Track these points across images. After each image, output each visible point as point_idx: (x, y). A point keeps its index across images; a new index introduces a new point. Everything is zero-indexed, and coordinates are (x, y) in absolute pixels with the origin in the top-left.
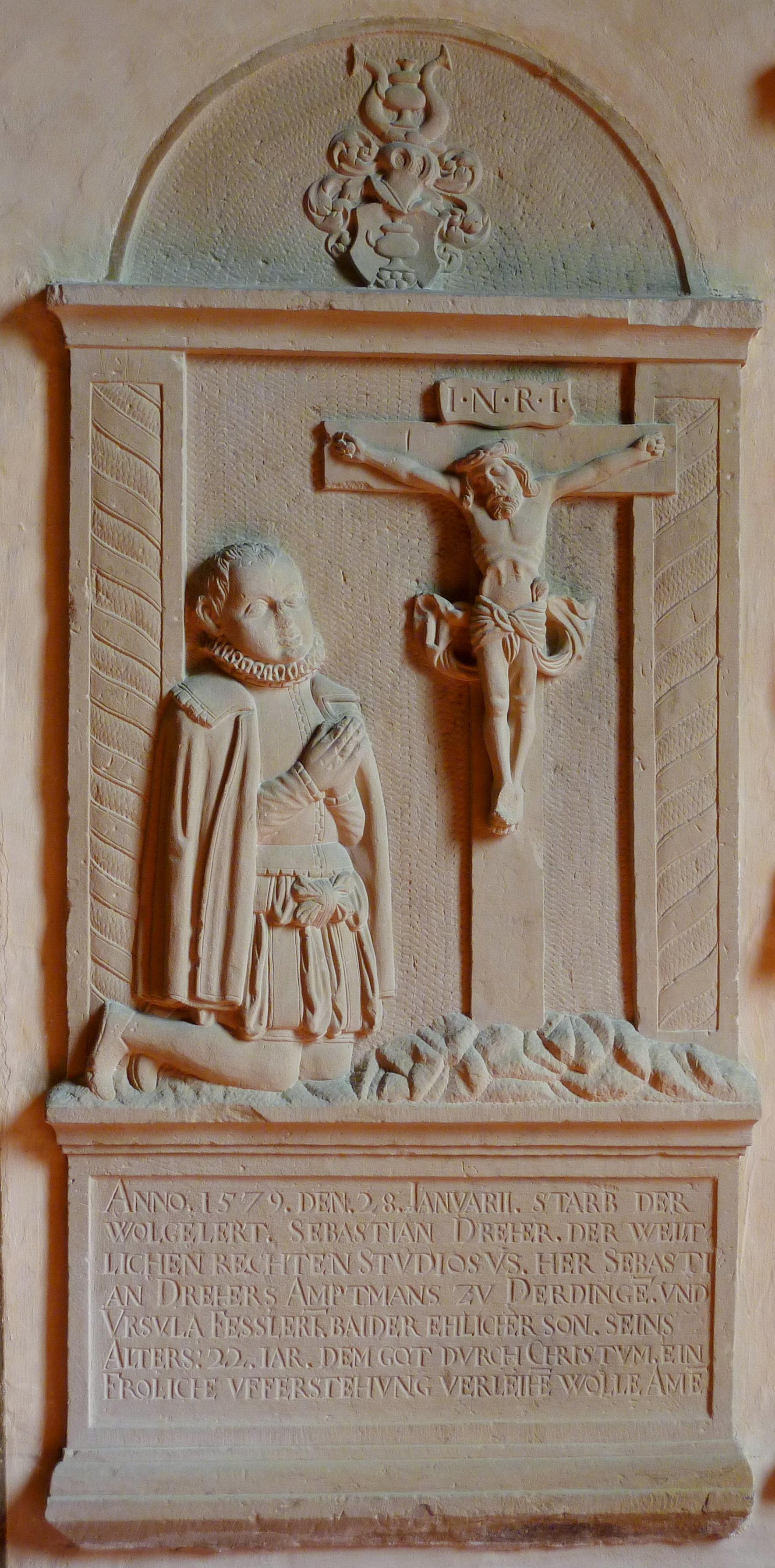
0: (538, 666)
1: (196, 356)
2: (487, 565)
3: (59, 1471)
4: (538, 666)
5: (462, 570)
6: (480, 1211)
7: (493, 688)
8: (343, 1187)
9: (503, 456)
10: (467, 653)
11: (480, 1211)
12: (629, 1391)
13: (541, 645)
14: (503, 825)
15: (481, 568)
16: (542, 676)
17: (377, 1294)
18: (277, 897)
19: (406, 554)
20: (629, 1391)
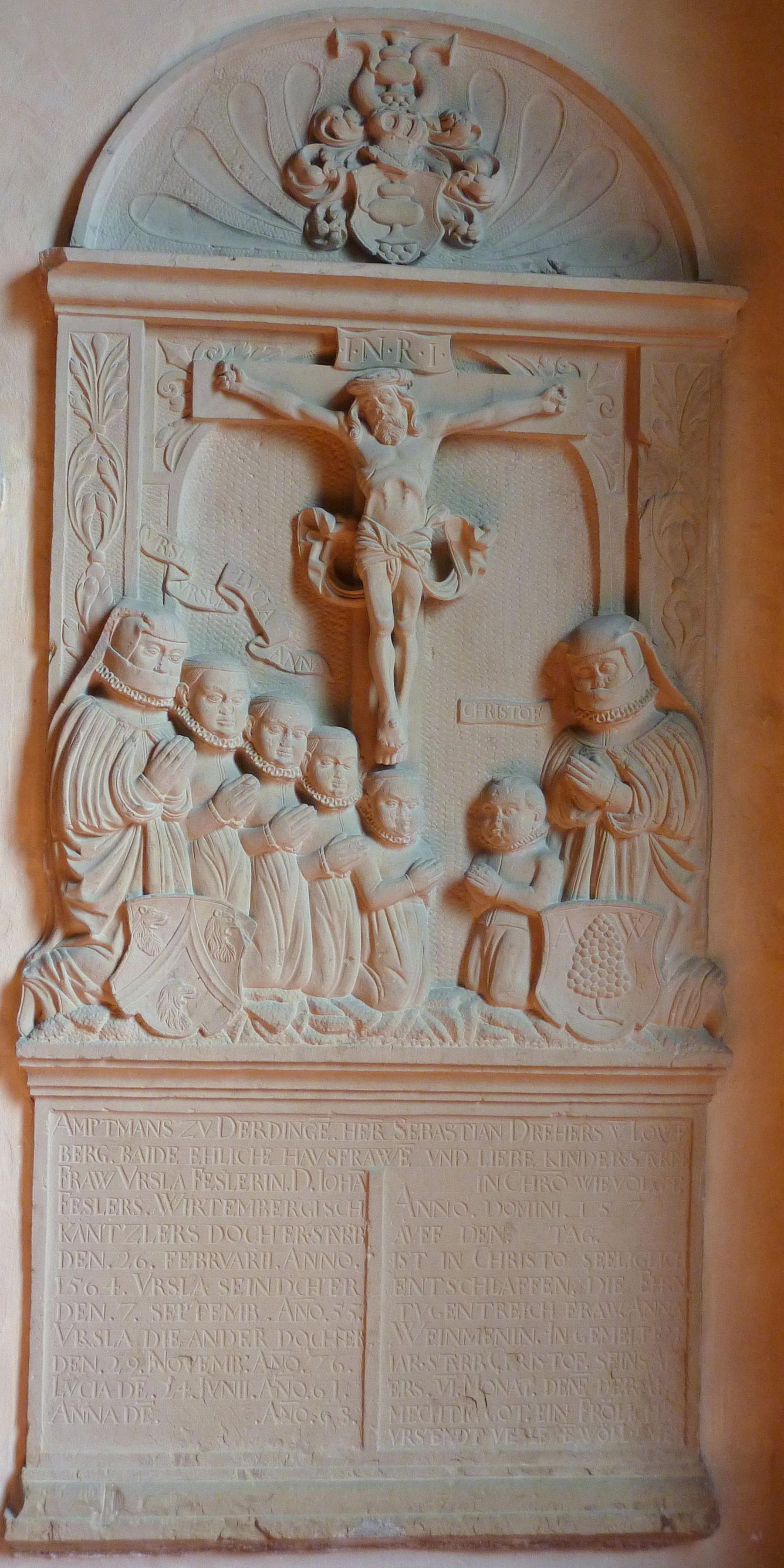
0: (424, 587)
1: (151, 325)
2: (370, 489)
3: (25, 1470)
4: (424, 587)
5: (344, 495)
6: (406, 1370)
7: (377, 609)
8: (123, 1118)
9: (389, 388)
10: (347, 575)
11: (406, 1370)
12: (107, 1213)
13: (428, 571)
14: (433, 542)
15: (364, 491)
16: (430, 604)
17: (471, 1382)
18: (85, 363)
19: (292, 482)
20: (107, 1213)
